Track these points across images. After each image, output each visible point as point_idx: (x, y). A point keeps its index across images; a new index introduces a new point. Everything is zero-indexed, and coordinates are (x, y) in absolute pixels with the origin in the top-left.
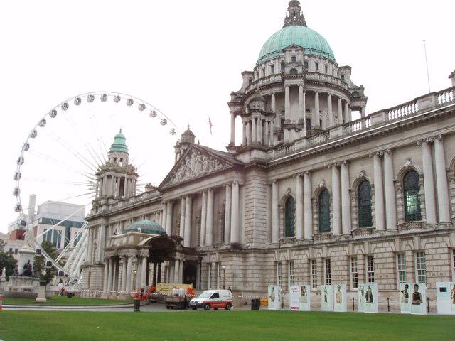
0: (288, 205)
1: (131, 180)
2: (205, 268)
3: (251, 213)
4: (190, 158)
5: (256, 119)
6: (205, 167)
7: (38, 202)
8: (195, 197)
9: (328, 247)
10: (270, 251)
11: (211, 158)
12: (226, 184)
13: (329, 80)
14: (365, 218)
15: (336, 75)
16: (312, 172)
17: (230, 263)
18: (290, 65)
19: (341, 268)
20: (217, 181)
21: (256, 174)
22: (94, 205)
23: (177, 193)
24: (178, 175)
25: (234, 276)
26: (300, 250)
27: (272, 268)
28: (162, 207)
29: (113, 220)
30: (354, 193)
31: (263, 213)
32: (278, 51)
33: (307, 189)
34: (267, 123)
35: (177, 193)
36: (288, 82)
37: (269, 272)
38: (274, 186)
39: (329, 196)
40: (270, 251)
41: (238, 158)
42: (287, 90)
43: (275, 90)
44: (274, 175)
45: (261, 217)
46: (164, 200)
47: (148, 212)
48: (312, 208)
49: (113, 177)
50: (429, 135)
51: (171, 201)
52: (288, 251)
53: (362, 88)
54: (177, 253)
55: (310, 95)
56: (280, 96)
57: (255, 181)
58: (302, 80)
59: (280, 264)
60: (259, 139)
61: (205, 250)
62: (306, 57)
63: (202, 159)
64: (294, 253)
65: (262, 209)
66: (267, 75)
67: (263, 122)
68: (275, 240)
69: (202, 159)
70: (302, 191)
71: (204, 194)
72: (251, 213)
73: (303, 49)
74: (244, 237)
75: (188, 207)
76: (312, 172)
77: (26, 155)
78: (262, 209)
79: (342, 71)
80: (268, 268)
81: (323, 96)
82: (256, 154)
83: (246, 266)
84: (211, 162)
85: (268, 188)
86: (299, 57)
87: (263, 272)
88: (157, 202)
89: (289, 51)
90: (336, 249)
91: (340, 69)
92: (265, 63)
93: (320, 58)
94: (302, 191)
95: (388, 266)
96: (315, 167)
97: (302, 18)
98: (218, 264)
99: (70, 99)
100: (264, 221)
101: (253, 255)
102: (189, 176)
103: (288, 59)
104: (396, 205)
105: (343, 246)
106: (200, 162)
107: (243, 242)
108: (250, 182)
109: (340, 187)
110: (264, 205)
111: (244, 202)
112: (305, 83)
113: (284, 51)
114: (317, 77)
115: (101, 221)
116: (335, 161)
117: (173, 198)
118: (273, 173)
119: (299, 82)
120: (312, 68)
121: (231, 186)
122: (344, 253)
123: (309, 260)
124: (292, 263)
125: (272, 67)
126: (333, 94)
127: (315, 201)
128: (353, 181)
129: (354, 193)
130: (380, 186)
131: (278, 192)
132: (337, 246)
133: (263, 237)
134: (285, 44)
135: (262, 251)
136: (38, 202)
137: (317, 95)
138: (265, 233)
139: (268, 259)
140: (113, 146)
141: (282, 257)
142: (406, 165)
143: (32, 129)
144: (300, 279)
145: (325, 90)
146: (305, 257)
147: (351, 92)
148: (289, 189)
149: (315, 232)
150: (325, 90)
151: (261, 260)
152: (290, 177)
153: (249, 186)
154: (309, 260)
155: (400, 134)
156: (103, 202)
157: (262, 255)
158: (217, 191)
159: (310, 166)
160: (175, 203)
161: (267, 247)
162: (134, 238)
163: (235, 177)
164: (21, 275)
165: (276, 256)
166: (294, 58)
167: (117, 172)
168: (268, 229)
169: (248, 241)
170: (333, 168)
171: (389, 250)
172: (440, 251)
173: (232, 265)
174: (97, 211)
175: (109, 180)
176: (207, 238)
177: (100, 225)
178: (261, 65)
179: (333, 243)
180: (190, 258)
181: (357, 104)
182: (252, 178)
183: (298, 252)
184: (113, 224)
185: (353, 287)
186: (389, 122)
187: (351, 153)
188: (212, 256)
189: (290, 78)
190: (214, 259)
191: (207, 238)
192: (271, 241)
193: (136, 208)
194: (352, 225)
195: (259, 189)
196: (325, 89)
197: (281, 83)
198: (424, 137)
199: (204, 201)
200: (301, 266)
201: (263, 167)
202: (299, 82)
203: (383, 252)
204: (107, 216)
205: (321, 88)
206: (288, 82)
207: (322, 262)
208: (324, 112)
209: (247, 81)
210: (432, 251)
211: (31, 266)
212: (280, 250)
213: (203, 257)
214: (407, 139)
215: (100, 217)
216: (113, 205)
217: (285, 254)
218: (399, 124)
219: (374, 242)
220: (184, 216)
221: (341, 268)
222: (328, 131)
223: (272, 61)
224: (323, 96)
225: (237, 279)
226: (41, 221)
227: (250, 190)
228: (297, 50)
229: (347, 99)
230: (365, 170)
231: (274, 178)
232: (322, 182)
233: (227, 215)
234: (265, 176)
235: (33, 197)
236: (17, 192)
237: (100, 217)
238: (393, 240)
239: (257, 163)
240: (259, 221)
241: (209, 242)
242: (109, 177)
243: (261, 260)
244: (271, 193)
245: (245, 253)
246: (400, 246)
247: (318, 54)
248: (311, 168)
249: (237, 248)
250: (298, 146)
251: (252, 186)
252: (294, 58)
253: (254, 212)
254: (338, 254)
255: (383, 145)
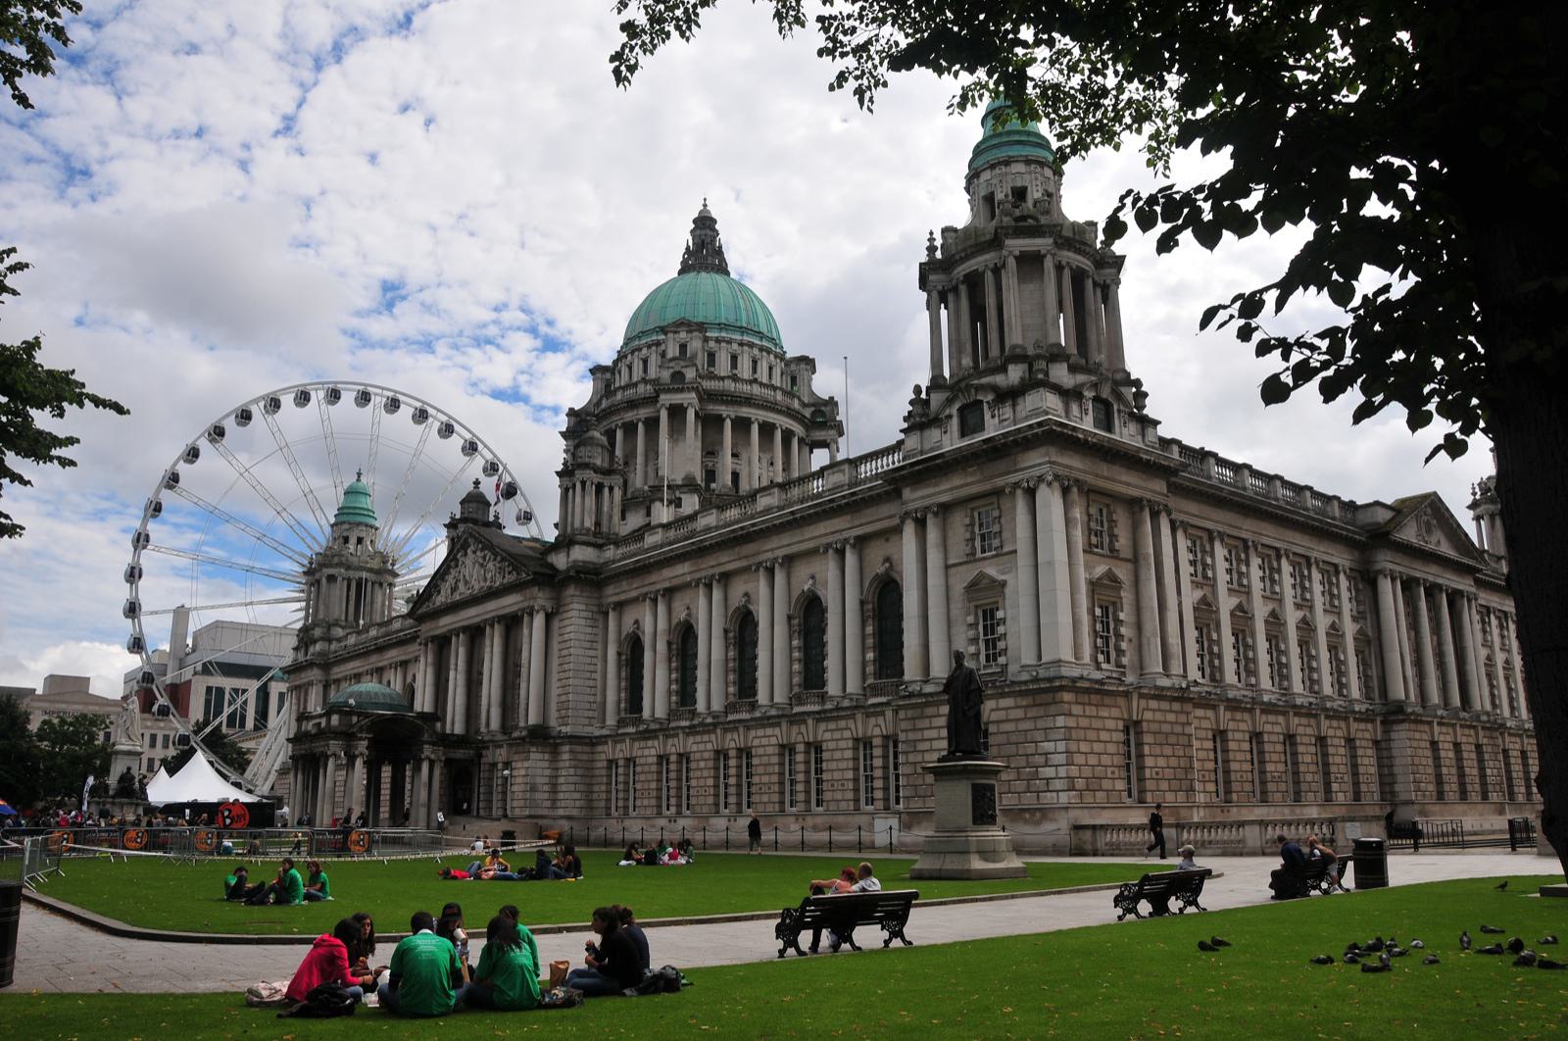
0: (633, 652)
1: (381, 584)
2: (487, 775)
3: (566, 667)
4: (466, 554)
5: (583, 483)
6: (489, 576)
7: (196, 623)
8: (475, 634)
9: (688, 734)
10: (601, 740)
11: (499, 558)
12: (523, 610)
13: (756, 390)
14: (812, 675)
15: (777, 381)
16: (789, 561)
17: (526, 764)
18: (671, 365)
19: (705, 773)
20: (510, 603)
21: (578, 593)
22: (301, 640)
23: (446, 622)
24: (445, 588)
25: (533, 789)
26: (648, 739)
27: (604, 772)
28: (413, 649)
29: (338, 672)
30: (731, 635)
31: (592, 668)
32: (654, 331)
33: (662, 625)
34: (606, 490)
35: (446, 622)
36: (666, 399)
37: (599, 780)
38: (612, 616)
39: (823, 611)
40: (601, 740)
41: (549, 560)
42: (664, 415)
43: (644, 413)
44: (612, 593)
45: (588, 675)
46: (423, 636)
47: (403, 658)
48: (670, 661)
49: (340, 579)
50: (837, 537)
51: (434, 639)
52: (810, 722)
53: (832, 402)
54: (426, 746)
55: (710, 424)
56: (652, 424)
57: (575, 606)
58: (694, 395)
59: (726, 757)
60: (589, 523)
61: (486, 738)
62: (712, 344)
63: (484, 558)
64: (637, 745)
65: (589, 660)
66: (635, 379)
67: (599, 488)
68: (611, 721)
69: (484, 558)
70: (654, 624)
71: (488, 629)
72: (566, 667)
73: (701, 327)
74: (553, 714)
75: (462, 651)
76: (789, 561)
77: (153, 528)
78: (589, 660)
79: (793, 367)
80: (597, 772)
81: (742, 425)
82: (581, 554)
83: (557, 769)
84: (498, 565)
85: (600, 618)
86: (695, 345)
87: (588, 781)
88: (413, 639)
89: (676, 332)
90: (698, 738)
91: (788, 363)
92: (632, 353)
93: (741, 344)
94: (654, 624)
95: (770, 769)
96: (676, 582)
97: (719, 252)
98: (507, 765)
99: (256, 401)
100: (591, 683)
101: (567, 748)
102: (463, 592)
103: (673, 351)
104: (791, 660)
105: (708, 732)
106: (482, 565)
107: (553, 722)
108: (567, 608)
109: (709, 617)
110: (592, 653)
111: (555, 646)
112: (701, 399)
113: (663, 330)
114: (730, 385)
115: (315, 674)
116: (703, 574)
117: (438, 632)
118: (610, 590)
119: (689, 399)
120: (723, 366)
121: (531, 615)
122: (709, 746)
123: (856, 740)
124: (819, 749)
125: (645, 362)
126: (761, 419)
127: (731, 635)
128: (795, 595)
129: (795, 622)
130: (768, 625)
131: (726, 599)
132: (698, 733)
133: (590, 714)
134: (671, 316)
135: (588, 741)
136: (196, 623)
137: (728, 424)
138: (594, 706)
139: (597, 757)
140: (342, 512)
141: (621, 751)
142: (806, 588)
143: (190, 441)
144: (646, 794)
145: (745, 412)
146: (653, 752)
147: (807, 413)
148: (887, 560)
149: (673, 706)
150: (745, 412)
151: (585, 757)
152: (635, 600)
153: (565, 615)
154: (856, 740)
155: (797, 531)
156: (318, 632)
157: (586, 749)
158: (512, 624)
159: (664, 580)
160: (442, 643)
161: (597, 733)
162: (340, 719)
163: (541, 598)
164: (113, 797)
165: (606, 751)
166: (683, 347)
167: (348, 568)
168: (599, 699)
169: (560, 721)
170: (1019, 492)
171: (774, 741)
172: (843, 744)
173: (532, 767)
174: (306, 654)
175: (332, 586)
176: (491, 716)
177: (310, 684)
178: (626, 356)
179: (694, 726)
180: (460, 754)
181: (819, 435)
182: (569, 600)
183: (643, 744)
184: (338, 681)
185: (867, 804)
186: (856, 484)
187: (727, 561)
188: (498, 751)
189: (669, 391)
190: (501, 755)
191: (491, 716)
192: (604, 721)
193: (380, 649)
194: (727, 695)
195: (583, 622)
196: (745, 409)
197: (652, 400)
198: (830, 539)
199: (488, 642)
200: (646, 768)
201: (591, 578)
202: (689, 399)
203: (838, 740)
204: (326, 664)
205: (736, 408)
206: (666, 399)
207: (807, 752)
208: (744, 456)
209: (601, 385)
210: (832, 745)
211: (133, 778)
212: (616, 738)
213: (484, 752)
214: (806, 540)
215: (310, 665)
216: (339, 640)
217: (803, 728)
218: (792, 513)
219: (756, 728)
220: (456, 670)
221: (705, 773)
222: (753, 496)
223: (645, 351)
224: (742, 425)
225: (538, 796)
226: (199, 668)
227: (566, 623)
228: (691, 332)
229: (798, 429)
230: (750, 591)
231: (611, 599)
232: (811, 582)
233: (524, 670)
234: (596, 595)
235: (181, 614)
236: (132, 610)
237: (310, 665)
238: (778, 725)
239: (577, 572)
240: (581, 682)
241: (495, 724)
242: (331, 578)
243: (585, 757)
244: (606, 628)
245: (556, 745)
246: (789, 735)
247: (737, 337)
248: (667, 585)
249: (541, 736)
250: (763, 502)
251: (569, 614)
252: (683, 347)
253: (571, 666)
254: (702, 747)
255: (772, 550)
